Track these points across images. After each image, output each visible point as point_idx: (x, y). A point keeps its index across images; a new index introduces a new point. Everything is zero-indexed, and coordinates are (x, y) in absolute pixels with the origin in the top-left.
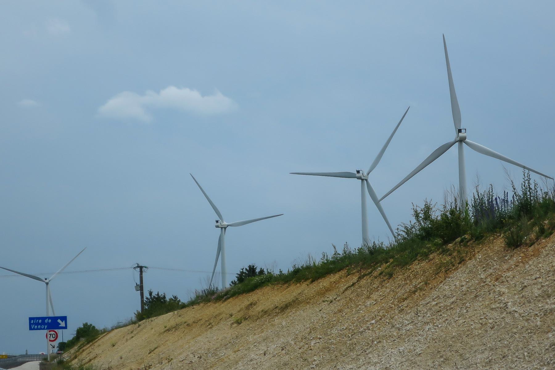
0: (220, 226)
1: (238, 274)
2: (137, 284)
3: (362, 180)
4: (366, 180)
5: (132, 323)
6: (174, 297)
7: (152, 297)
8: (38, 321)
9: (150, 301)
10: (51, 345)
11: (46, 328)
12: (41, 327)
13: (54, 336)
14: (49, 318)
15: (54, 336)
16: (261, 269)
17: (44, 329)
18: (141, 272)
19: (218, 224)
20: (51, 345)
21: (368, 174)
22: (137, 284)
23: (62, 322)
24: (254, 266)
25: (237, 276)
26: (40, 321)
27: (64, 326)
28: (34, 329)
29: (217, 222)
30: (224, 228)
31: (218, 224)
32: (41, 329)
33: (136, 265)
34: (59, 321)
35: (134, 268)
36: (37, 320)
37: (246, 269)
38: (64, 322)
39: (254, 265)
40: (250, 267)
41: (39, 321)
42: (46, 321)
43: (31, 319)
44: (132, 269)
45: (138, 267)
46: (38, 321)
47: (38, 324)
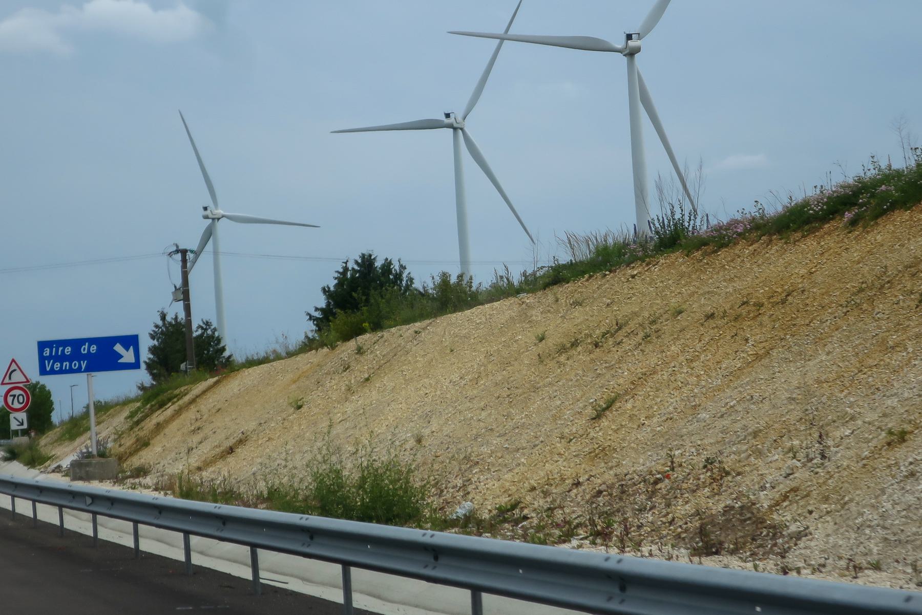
0: (210, 216)
1: (337, 272)
2: (175, 287)
3: (455, 129)
4: (462, 129)
5: (287, 353)
6: (204, 323)
7: (166, 322)
8: (63, 351)
9: (162, 330)
10: (14, 418)
11: (83, 367)
12: (70, 366)
13: (21, 400)
14: (92, 341)
15: (21, 400)
16: (387, 259)
17: (79, 370)
18: (184, 261)
19: (208, 213)
20: (14, 418)
21: (464, 118)
22: (175, 287)
23: (127, 349)
24: (370, 256)
25: (336, 275)
26: (68, 350)
27: (133, 361)
28: (53, 372)
29: (205, 209)
30: (216, 219)
31: (208, 213)
32: (71, 371)
33: (174, 248)
34: (118, 348)
35: (170, 254)
36: (61, 349)
37: (356, 262)
38: (131, 348)
39: (371, 252)
40: (363, 256)
41: (66, 351)
42: (84, 350)
43: (42, 345)
44: (166, 257)
45: (177, 251)
46: (63, 351)
47: (62, 358)
